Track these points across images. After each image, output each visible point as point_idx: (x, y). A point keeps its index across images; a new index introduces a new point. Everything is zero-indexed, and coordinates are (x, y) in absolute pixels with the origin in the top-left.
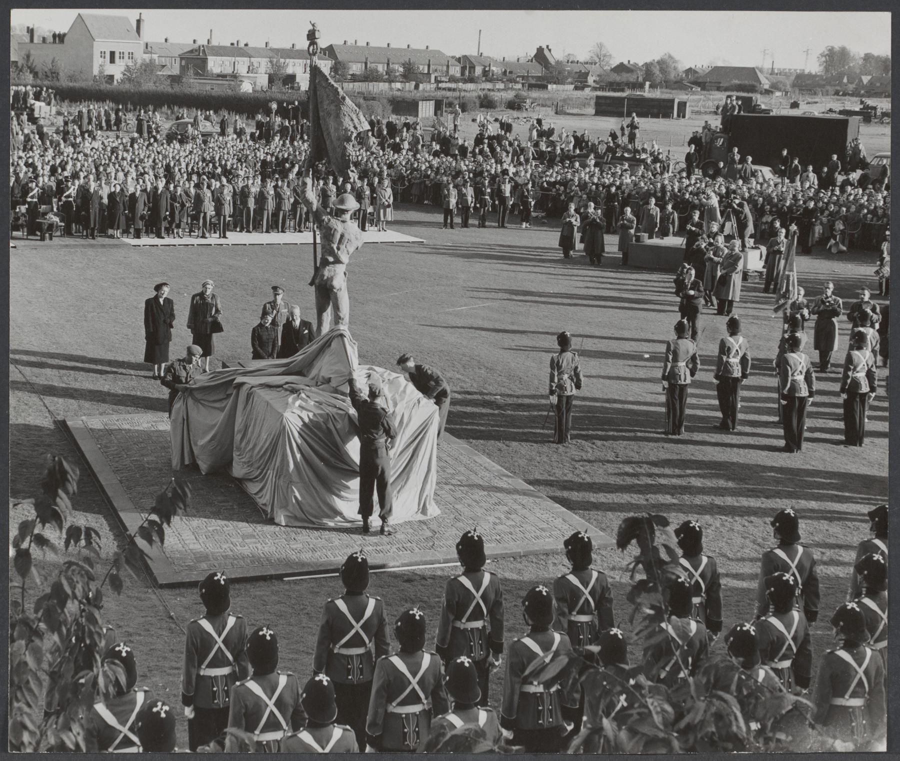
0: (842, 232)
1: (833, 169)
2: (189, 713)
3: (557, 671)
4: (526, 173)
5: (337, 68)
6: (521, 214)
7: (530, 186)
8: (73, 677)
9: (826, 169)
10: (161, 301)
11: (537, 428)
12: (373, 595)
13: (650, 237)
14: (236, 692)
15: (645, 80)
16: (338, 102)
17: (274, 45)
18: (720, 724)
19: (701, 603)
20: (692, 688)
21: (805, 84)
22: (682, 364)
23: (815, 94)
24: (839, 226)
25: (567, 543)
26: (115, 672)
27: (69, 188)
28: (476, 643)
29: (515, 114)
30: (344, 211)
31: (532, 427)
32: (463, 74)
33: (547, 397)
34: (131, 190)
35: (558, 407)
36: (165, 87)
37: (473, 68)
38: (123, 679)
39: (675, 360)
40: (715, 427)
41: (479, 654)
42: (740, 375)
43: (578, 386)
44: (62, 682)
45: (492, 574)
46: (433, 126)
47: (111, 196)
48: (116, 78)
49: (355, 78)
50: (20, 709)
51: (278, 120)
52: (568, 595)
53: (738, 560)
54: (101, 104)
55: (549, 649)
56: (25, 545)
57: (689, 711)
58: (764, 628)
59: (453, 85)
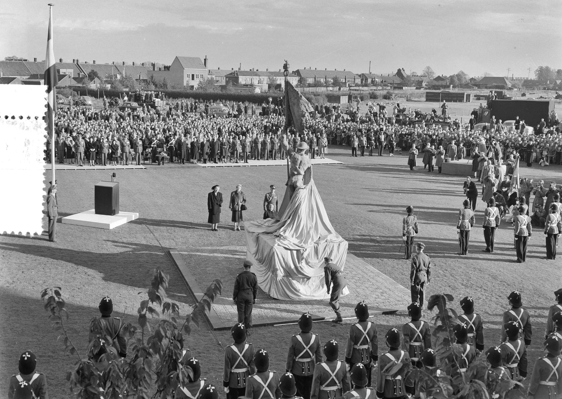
0: (547, 156)
1: (542, 125)
2: (226, 390)
3: (397, 370)
4: (391, 130)
5: (301, 81)
6: (390, 149)
7: (393, 136)
8: (167, 374)
9: (539, 126)
10: (216, 194)
11: (396, 252)
12: (314, 333)
13: (452, 160)
14: (249, 380)
15: (450, 84)
16: (299, 98)
17: (270, 70)
18: (477, 396)
19: (473, 336)
20: (464, 378)
21: (528, 84)
22: (467, 221)
23: (534, 89)
24: (545, 153)
25: (409, 308)
26: (187, 372)
27: (171, 140)
28: (365, 355)
29: (387, 101)
30: (302, 150)
31: (394, 252)
32: (362, 82)
33: (402, 237)
34: (202, 140)
35: (407, 242)
36: (218, 91)
37: (367, 79)
38: (192, 375)
39: (463, 219)
40: (483, 251)
41: (366, 361)
42: (495, 225)
43: (416, 232)
44: (162, 377)
45: (372, 323)
46: (348, 108)
47: (192, 144)
48: (195, 87)
49: (310, 85)
50: (141, 390)
51: (272, 106)
52: (410, 334)
53: (494, 315)
54: (187, 99)
55: (397, 358)
56: (143, 313)
57: (462, 390)
58: (504, 348)
59: (357, 88)
